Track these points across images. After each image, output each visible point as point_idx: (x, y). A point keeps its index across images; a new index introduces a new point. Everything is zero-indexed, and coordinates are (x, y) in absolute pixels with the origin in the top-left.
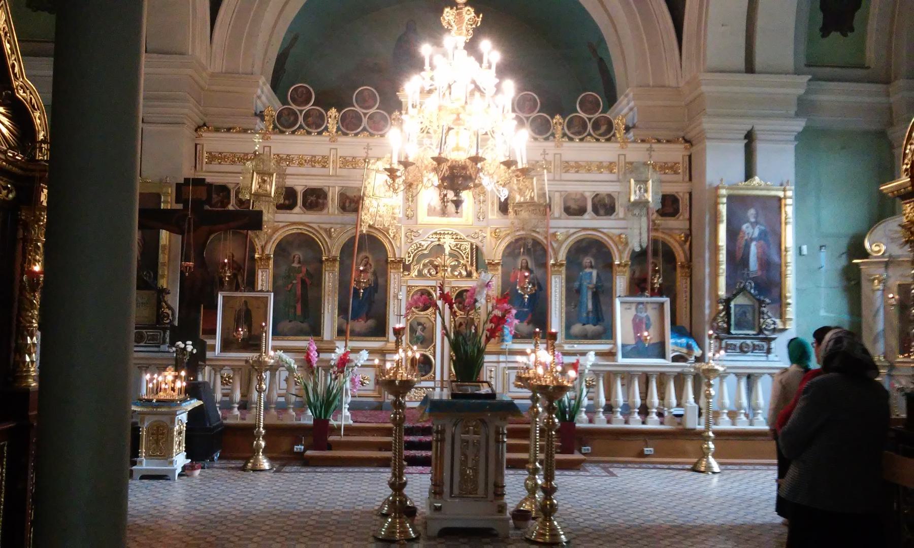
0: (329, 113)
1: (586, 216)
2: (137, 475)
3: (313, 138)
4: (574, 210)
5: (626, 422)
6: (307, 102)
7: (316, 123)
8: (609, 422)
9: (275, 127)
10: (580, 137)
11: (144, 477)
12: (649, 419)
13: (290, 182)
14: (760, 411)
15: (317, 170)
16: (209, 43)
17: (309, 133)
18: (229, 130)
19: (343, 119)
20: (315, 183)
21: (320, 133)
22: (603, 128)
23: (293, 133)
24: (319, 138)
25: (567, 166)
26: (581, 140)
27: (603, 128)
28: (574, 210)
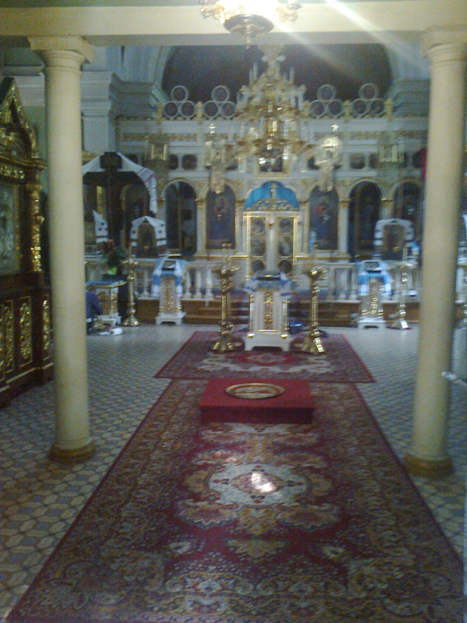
0: (197, 106)
1: (364, 169)
2: (361, 326)
3: (188, 122)
4: (358, 164)
5: (336, 299)
6: (183, 98)
7: (189, 112)
8: (192, 297)
9: (164, 116)
10: (191, 116)
11: (367, 327)
12: (194, 296)
13: (174, 151)
14: (352, 292)
15: (191, 143)
16: (120, 58)
17: (185, 119)
18: (135, 118)
19: (356, 106)
20: (190, 152)
21: (192, 119)
22: (378, 108)
23: (322, 117)
24: (191, 122)
25: (355, 136)
26: (175, 119)
27: (378, 108)
28: (358, 164)
